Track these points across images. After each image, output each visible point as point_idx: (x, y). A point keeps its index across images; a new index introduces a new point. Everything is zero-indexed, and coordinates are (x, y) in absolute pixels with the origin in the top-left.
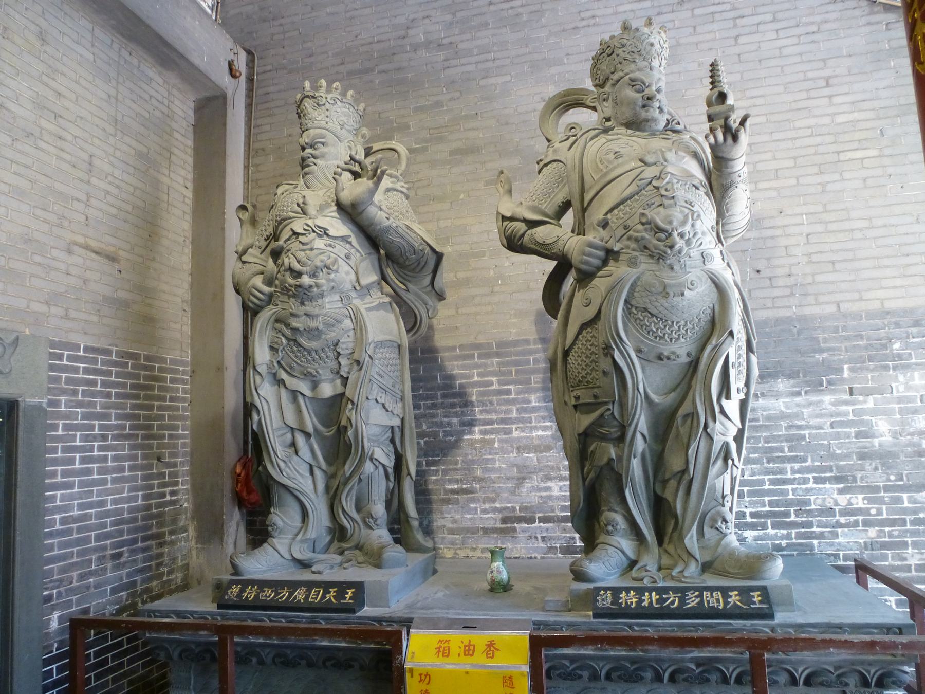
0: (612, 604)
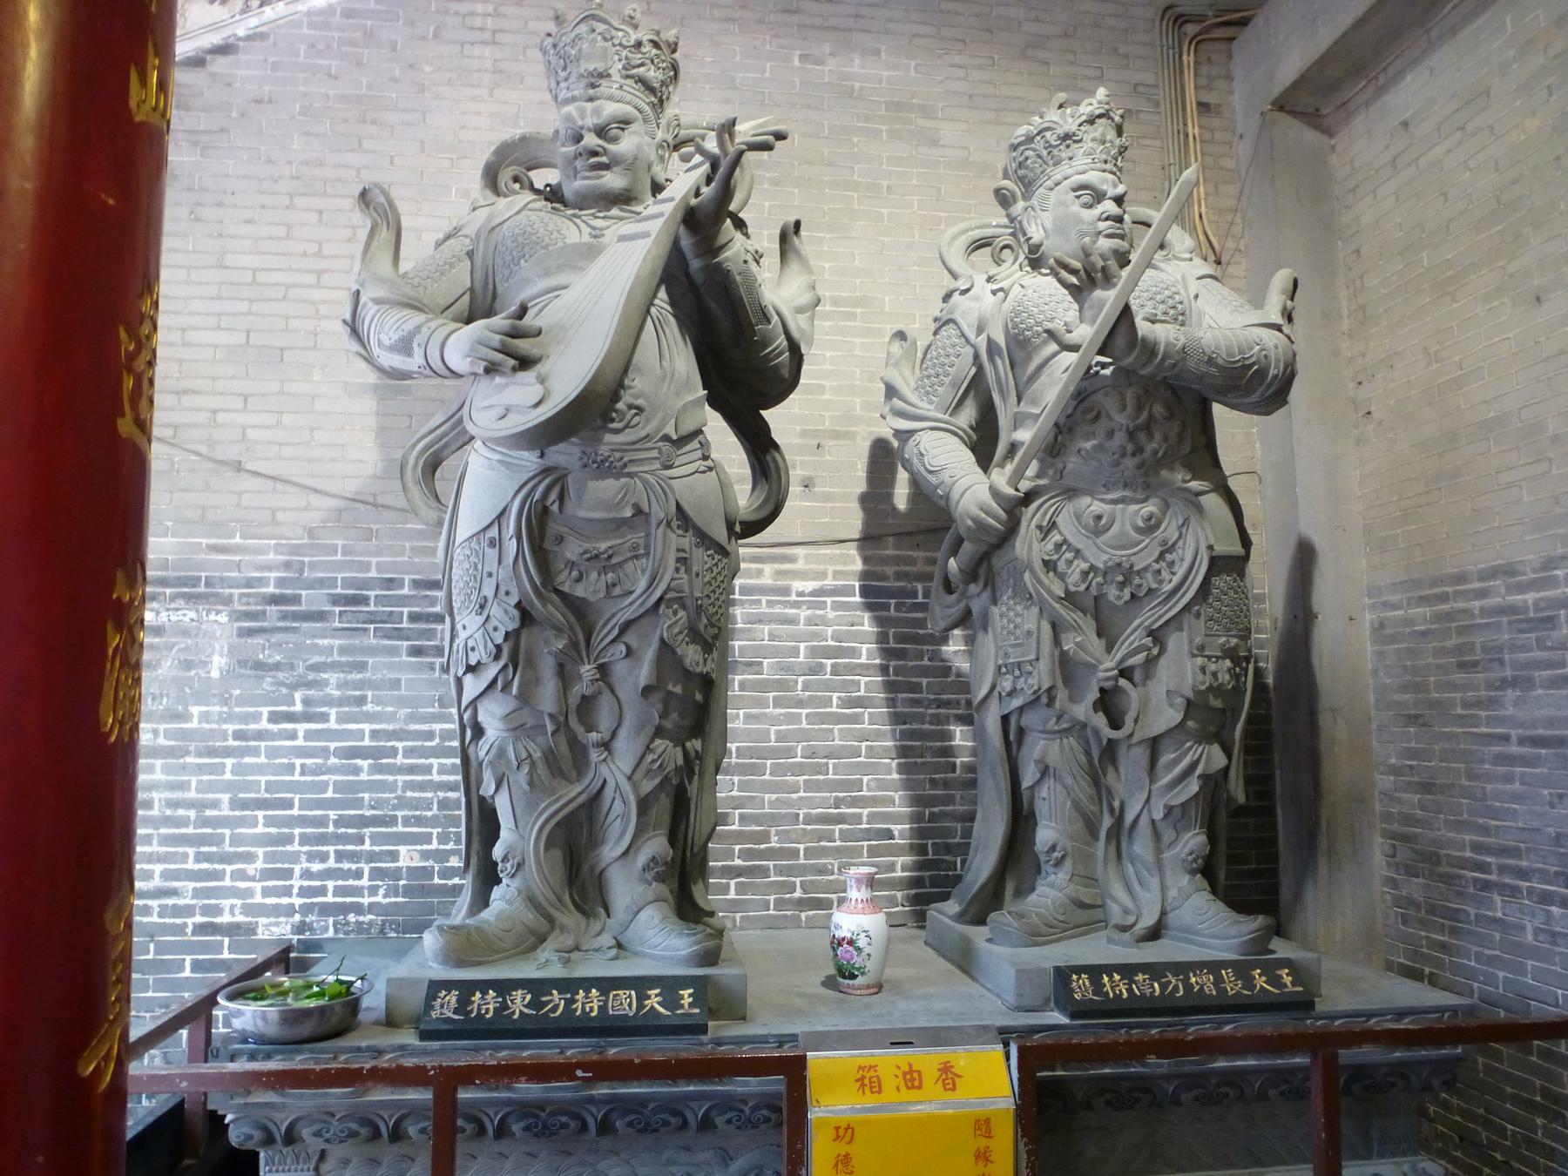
0: (456, 1011)
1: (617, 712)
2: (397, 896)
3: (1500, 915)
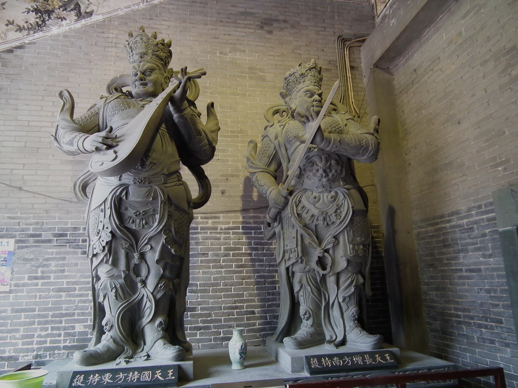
1: (147, 270)
2: (74, 342)
3: (465, 333)
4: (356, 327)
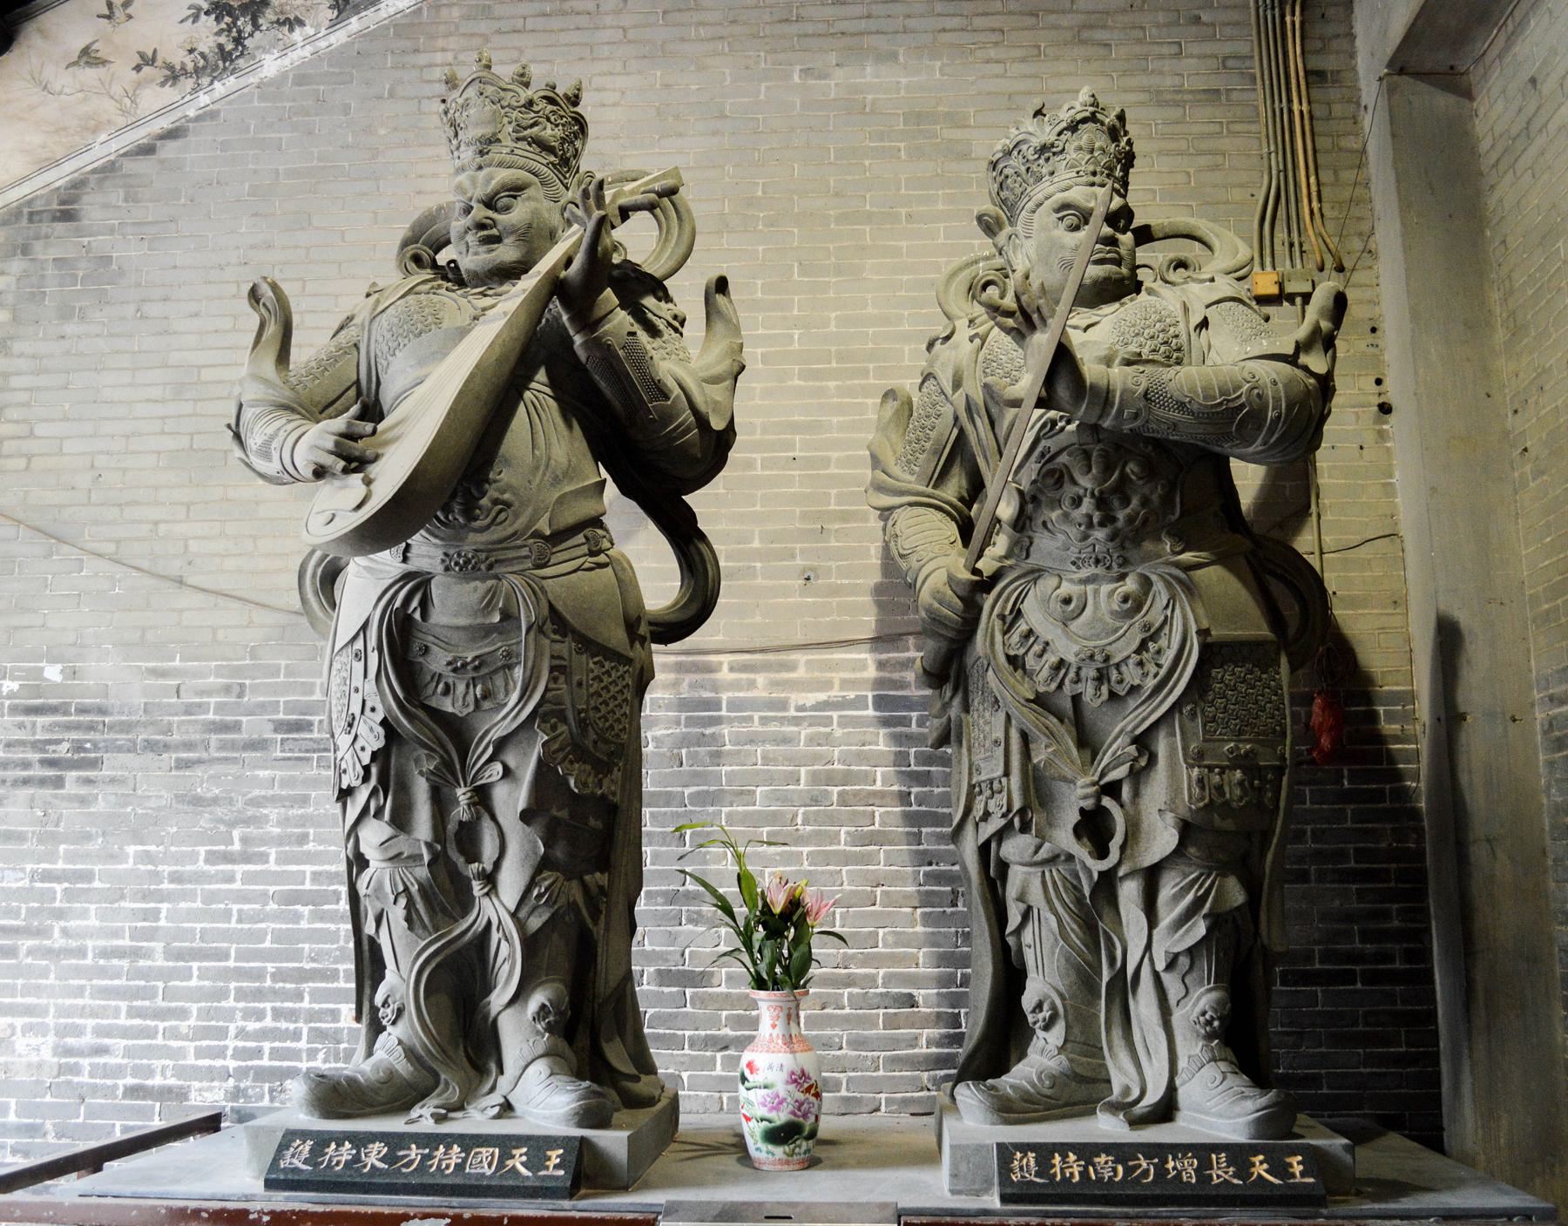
1: (497, 841)
4: (1214, 1059)
